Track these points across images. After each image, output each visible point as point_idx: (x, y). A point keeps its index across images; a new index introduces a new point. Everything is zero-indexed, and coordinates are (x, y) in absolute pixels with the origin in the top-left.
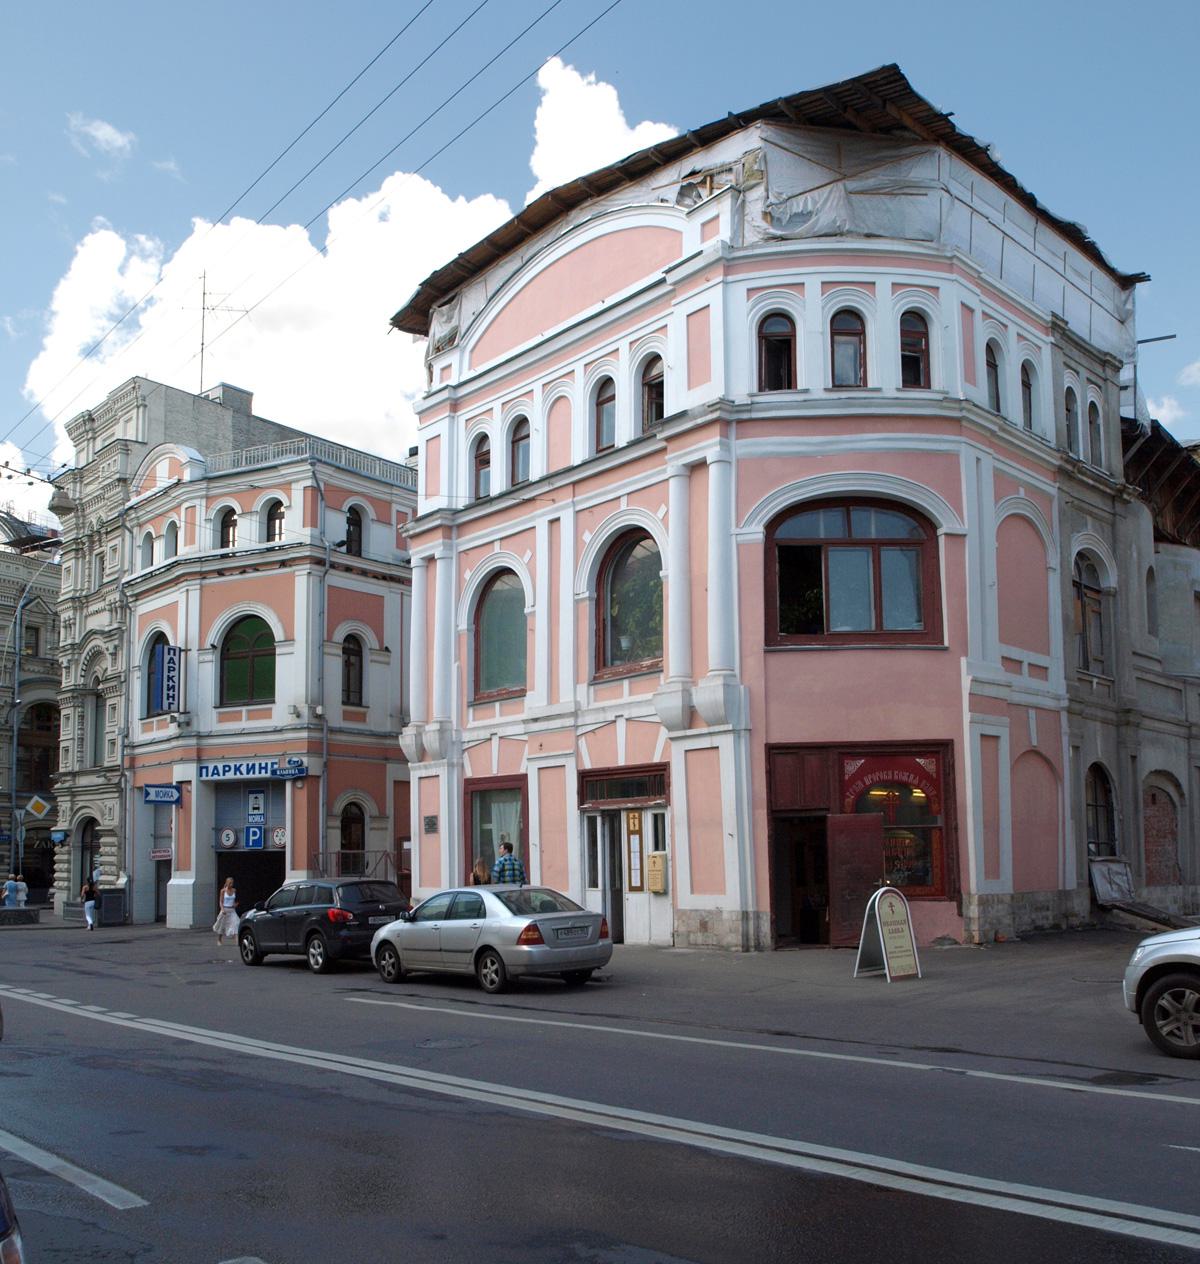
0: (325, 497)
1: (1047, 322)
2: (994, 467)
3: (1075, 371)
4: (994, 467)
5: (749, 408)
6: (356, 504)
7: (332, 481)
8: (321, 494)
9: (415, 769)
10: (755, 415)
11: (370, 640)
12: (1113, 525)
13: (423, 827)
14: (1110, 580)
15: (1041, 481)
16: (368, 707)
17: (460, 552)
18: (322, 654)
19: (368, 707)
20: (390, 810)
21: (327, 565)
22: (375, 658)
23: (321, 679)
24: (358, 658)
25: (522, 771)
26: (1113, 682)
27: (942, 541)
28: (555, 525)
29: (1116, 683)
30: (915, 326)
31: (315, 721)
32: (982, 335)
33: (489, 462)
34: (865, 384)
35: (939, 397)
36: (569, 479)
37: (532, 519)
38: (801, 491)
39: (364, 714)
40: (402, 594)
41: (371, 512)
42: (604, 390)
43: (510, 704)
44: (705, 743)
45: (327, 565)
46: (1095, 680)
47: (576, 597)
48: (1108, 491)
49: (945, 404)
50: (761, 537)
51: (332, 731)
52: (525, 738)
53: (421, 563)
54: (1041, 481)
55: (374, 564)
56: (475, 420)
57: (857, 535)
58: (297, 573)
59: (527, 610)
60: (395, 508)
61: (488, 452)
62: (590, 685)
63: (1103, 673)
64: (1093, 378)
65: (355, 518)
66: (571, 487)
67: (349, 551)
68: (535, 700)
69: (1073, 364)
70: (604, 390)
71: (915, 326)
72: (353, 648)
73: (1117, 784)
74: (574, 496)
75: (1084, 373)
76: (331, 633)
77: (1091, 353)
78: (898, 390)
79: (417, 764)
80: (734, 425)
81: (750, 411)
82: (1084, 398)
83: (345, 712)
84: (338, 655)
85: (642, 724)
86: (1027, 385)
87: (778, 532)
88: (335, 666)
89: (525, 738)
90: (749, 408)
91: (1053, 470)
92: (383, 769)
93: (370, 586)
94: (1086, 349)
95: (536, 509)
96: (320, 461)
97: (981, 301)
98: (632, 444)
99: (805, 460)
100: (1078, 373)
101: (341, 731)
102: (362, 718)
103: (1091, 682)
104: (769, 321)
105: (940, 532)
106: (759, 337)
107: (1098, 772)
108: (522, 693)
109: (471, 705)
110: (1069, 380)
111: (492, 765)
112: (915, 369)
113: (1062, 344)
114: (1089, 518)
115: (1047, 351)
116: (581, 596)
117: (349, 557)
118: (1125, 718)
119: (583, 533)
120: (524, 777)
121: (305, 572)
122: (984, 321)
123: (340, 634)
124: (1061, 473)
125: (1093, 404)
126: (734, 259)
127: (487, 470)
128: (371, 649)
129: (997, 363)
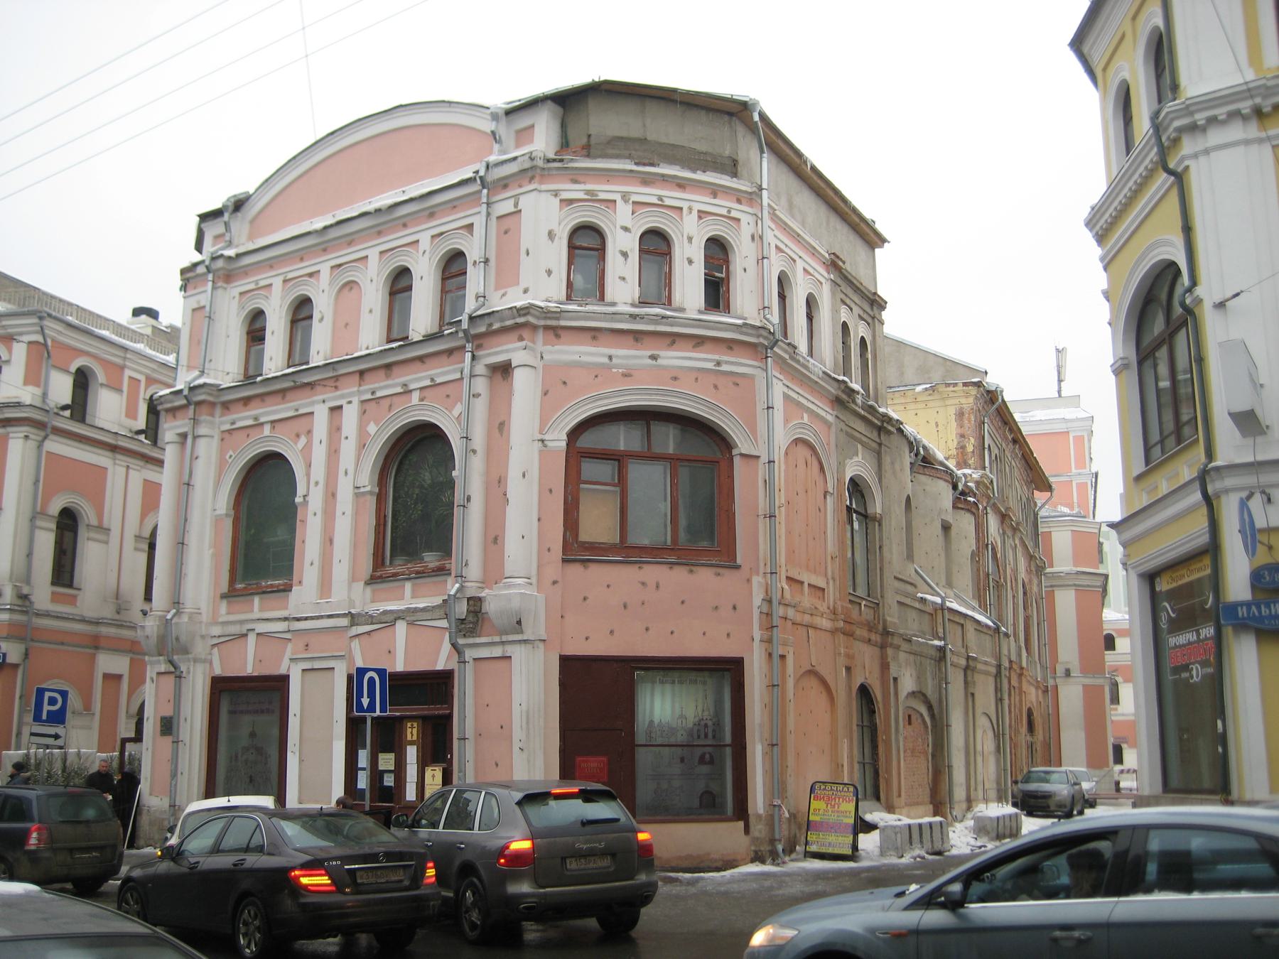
0: (51, 353)
1: (828, 261)
2: (784, 392)
3: (849, 307)
4: (784, 392)
5: (558, 315)
6: (83, 366)
7: (61, 338)
8: (48, 353)
9: (152, 663)
10: (563, 323)
11: (88, 514)
12: (879, 454)
13: (159, 728)
14: (877, 507)
15: (306, 267)
16: (79, 589)
17: (223, 432)
18: (33, 528)
19: (79, 589)
20: (97, 706)
21: (49, 430)
22: (92, 535)
23: (29, 555)
24: (1152, 833)
25: (283, 671)
26: (878, 604)
27: (737, 460)
28: (336, 413)
29: (881, 604)
30: (718, 250)
31: (19, 602)
32: (775, 265)
33: (264, 339)
34: (670, 303)
35: (739, 322)
36: (365, 368)
37: (313, 403)
38: (606, 401)
39: (75, 597)
40: (128, 466)
41: (101, 375)
42: (400, 282)
43: (272, 600)
44: (497, 652)
45: (49, 430)
46: (864, 603)
47: (357, 491)
48: (876, 421)
49: (744, 329)
50: (564, 444)
51: (39, 615)
52: (288, 636)
53: (176, 439)
54: (306, 267)
55: (102, 433)
56: (253, 293)
57: (657, 449)
58: (11, 435)
59: (298, 500)
60: (128, 373)
61: (264, 329)
62: (367, 583)
63: (869, 596)
64: (865, 316)
65: (82, 381)
66: (357, 377)
67: (72, 417)
68: (303, 597)
69: (848, 301)
70: (400, 282)
71: (718, 250)
72: (68, 522)
73: (881, 706)
74: (360, 385)
75: (856, 310)
76: (46, 502)
77: (862, 292)
78: (700, 312)
79: (155, 659)
80: (541, 331)
81: (558, 319)
82: (856, 332)
83: (53, 593)
84: (49, 530)
85: (423, 628)
86: (810, 317)
87: (581, 438)
88: (46, 542)
89: (288, 636)
90: (558, 315)
91: (831, 398)
92: (93, 659)
93: (69, 448)
94: (858, 289)
95: (316, 395)
96: (50, 315)
97: (775, 236)
98: (430, 338)
99: (598, 371)
100: (851, 309)
101: (47, 615)
102: (72, 600)
103: (860, 604)
104: (580, 233)
105: (735, 452)
106: (569, 247)
107: (864, 691)
108: (287, 589)
109: (223, 596)
110: (844, 315)
111: (248, 662)
112: (716, 292)
113: (839, 281)
114: (859, 446)
115: (827, 288)
116: (362, 490)
117: (71, 422)
118: (884, 638)
119: (368, 424)
120: (285, 679)
121: (22, 435)
122: (776, 254)
123: (55, 508)
124: (838, 402)
125: (862, 338)
126: (549, 169)
127: (261, 346)
128: (88, 525)
129: (786, 294)
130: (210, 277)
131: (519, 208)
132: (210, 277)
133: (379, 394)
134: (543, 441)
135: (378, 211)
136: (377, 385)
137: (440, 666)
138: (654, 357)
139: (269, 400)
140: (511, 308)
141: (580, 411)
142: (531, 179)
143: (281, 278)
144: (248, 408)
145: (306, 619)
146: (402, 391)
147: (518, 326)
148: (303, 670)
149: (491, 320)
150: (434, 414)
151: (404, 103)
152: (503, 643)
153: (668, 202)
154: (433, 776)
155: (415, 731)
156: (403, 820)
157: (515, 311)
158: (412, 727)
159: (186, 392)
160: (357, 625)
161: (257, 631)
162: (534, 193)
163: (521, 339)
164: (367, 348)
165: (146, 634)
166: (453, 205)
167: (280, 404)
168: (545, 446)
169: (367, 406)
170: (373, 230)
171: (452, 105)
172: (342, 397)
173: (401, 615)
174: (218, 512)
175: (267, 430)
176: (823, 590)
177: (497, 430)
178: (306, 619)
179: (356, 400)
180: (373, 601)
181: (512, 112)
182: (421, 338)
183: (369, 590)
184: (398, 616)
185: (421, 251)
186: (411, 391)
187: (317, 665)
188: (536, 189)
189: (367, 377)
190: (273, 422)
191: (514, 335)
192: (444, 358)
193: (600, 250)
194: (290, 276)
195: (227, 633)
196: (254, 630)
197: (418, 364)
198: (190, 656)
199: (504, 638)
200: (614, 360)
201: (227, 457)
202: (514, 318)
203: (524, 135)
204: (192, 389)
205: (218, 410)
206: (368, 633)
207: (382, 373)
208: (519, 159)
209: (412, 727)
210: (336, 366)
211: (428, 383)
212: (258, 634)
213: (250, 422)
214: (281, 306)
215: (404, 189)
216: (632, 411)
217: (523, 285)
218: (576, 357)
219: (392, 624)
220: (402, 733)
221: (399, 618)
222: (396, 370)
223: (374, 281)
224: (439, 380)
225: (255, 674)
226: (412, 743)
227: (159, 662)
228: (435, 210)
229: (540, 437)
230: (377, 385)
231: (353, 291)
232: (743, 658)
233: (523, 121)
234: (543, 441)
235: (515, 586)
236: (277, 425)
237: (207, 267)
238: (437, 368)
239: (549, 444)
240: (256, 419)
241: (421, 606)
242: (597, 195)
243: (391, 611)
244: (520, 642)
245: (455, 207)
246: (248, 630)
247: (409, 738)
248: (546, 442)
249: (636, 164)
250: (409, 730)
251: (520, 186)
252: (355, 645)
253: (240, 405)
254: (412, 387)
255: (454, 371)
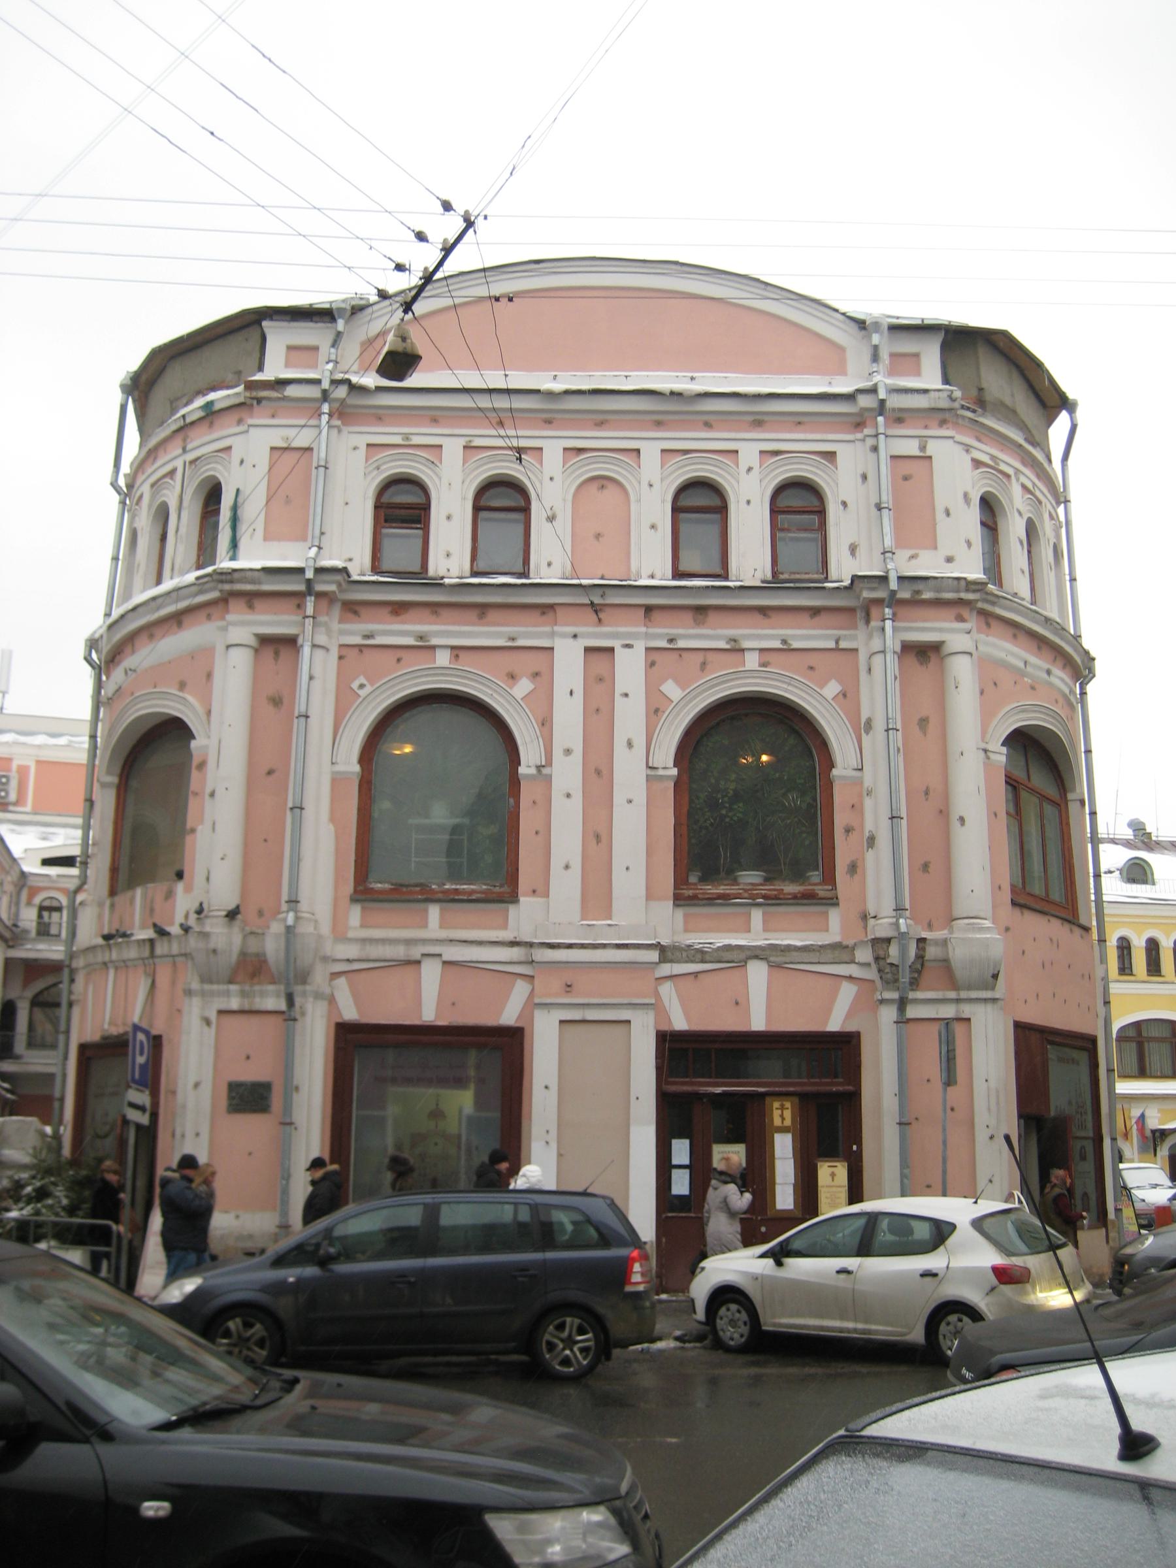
10: (998, 611)
13: (223, 1102)
25: (509, 1017)
37: (552, 635)
66: (642, 612)
81: (993, 604)
105: (1070, 796)
116: (661, 772)
130: (326, 408)
131: (928, 454)
132: (326, 408)
133: (681, 644)
134: (985, 751)
135: (675, 395)
136: (681, 631)
137: (834, 1025)
138: (1049, 672)
139: (445, 613)
140: (958, 579)
141: (382, 697)
142: (943, 423)
143: (462, 442)
144: (399, 618)
145: (570, 946)
146: (728, 647)
147: (961, 602)
148: (561, 1022)
149: (920, 586)
150: (790, 688)
151: (681, 260)
152: (958, 1001)
153: (416, 440)
154: (833, 1175)
155: (788, 1114)
156: (892, 1231)
157: (963, 583)
158: (782, 1108)
159: (309, 574)
160: (671, 961)
161: (445, 958)
162: (950, 442)
163: (960, 619)
164: (652, 577)
165: (212, 945)
166: (799, 421)
167: (474, 624)
168: (988, 758)
169: (656, 656)
170: (648, 417)
171: (769, 288)
172: (615, 636)
173: (758, 952)
174: (340, 768)
175: (443, 659)
176: (897, 966)
177: (917, 728)
178: (570, 946)
179: (640, 646)
180: (686, 930)
181: (899, 329)
182: (758, 584)
183: (680, 913)
184: (756, 954)
185: (743, 467)
186: (743, 650)
187: (592, 1015)
188: (952, 438)
189: (656, 615)
190: (453, 648)
191: (951, 612)
192: (805, 618)
193: (721, 509)
194: (478, 442)
195: (388, 957)
196: (440, 955)
197: (758, 617)
198: (308, 988)
199: (964, 994)
200: (1029, 669)
201: (355, 685)
202: (958, 591)
203: (907, 362)
204: (320, 571)
205: (336, 611)
206: (696, 974)
207: (688, 617)
208: (932, 394)
209: (782, 1108)
210: (608, 591)
211: (777, 644)
212: (445, 963)
213: (410, 641)
214: (463, 482)
215: (695, 375)
216: (703, 714)
217: (943, 552)
218: (1002, 655)
219: (742, 964)
220: (763, 1116)
221: (756, 957)
222: (712, 617)
223: (657, 486)
224: (796, 644)
225: (441, 1023)
226: (783, 1130)
227: (227, 994)
228: (766, 418)
229: (983, 746)
230: (681, 631)
231: (605, 492)
232: (1096, 1037)
233: (907, 345)
234: (985, 751)
235: (981, 929)
236: (462, 654)
237: (325, 392)
238: (792, 628)
239: (992, 756)
240: (421, 638)
241: (799, 943)
242: (998, 464)
243: (740, 948)
244: (985, 1000)
245: (799, 423)
246: (424, 955)
247: (777, 1121)
248: (989, 754)
249: (1026, 439)
250: (776, 1114)
251: (926, 427)
252: (666, 990)
253: (384, 612)
254: (746, 644)
255: (826, 637)
